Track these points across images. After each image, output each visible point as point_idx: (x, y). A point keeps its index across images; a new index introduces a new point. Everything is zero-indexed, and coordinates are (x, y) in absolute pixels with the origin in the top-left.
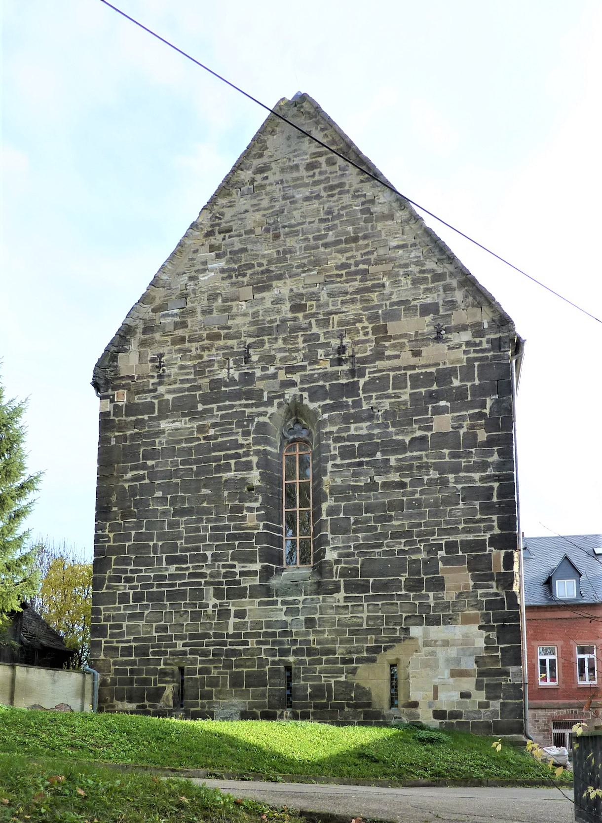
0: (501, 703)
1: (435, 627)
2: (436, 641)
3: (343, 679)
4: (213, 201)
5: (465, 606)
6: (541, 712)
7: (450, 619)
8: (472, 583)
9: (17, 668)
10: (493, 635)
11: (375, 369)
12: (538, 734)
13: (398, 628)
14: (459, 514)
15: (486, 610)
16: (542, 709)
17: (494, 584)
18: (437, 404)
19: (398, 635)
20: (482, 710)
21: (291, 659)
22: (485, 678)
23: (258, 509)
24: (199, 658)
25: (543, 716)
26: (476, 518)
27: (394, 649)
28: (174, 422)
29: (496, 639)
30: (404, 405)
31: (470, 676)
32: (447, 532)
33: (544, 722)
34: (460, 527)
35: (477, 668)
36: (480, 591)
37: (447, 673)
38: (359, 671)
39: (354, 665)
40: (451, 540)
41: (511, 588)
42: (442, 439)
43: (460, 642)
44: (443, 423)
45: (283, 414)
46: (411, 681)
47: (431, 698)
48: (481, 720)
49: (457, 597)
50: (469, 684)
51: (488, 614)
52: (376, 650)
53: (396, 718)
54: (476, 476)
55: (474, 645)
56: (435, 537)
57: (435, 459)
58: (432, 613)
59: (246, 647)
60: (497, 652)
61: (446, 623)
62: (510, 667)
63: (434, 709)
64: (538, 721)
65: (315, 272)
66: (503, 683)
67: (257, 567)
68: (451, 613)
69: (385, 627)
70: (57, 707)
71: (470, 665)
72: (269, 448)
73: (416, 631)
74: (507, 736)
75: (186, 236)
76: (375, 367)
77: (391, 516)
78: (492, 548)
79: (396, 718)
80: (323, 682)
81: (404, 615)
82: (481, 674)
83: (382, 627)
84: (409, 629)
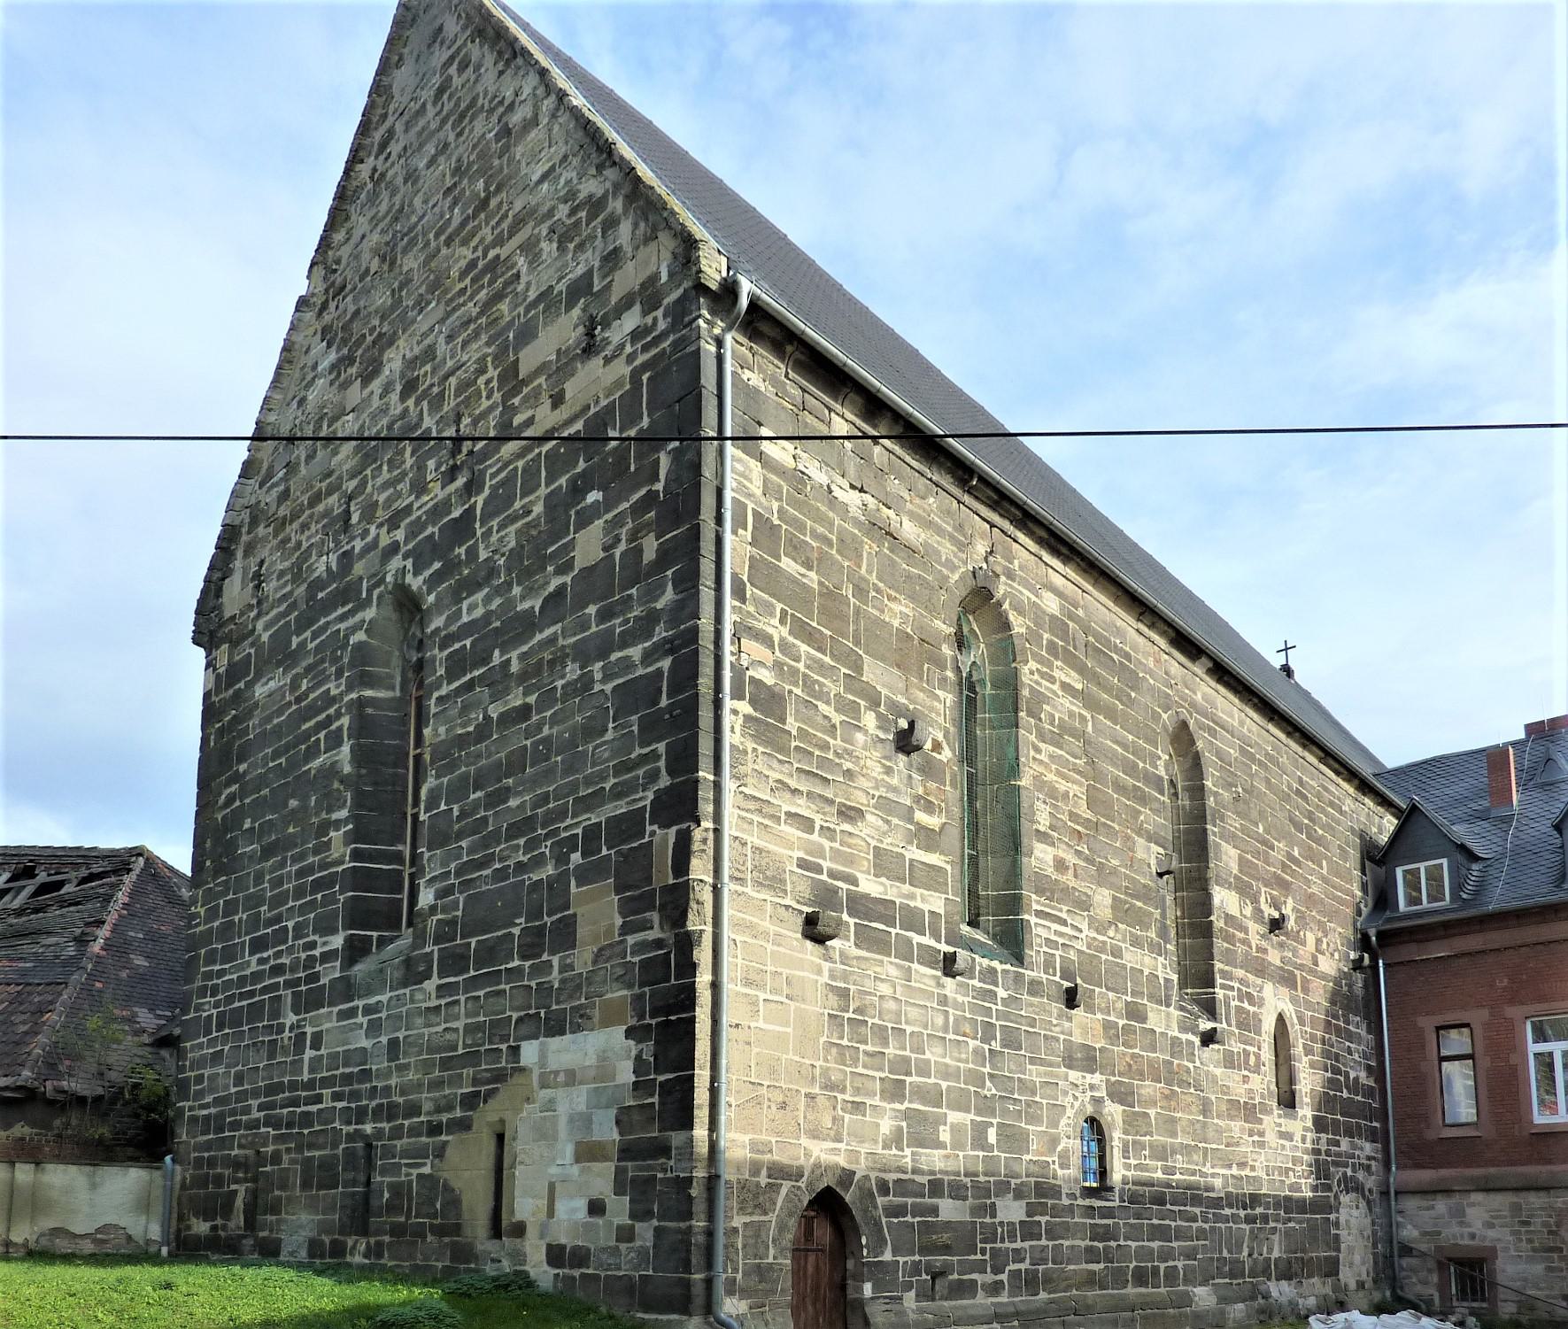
0: (657, 1229)
1: (557, 1039)
2: (556, 1073)
3: (427, 1170)
4: (325, 244)
5: (605, 981)
6: (1536, 1200)
7: (582, 1016)
8: (619, 921)
9: (17, 1165)
10: (648, 1049)
11: (500, 464)
12: (1530, 1260)
13: (504, 1047)
14: (606, 755)
15: (640, 987)
16: (1538, 1189)
17: (655, 917)
18: (582, 505)
19: (504, 1064)
20: (623, 1246)
21: (368, 1128)
22: (630, 1164)
23: (346, 821)
24: (272, 1132)
25: (1542, 1209)
26: (632, 756)
27: (501, 1096)
28: (266, 683)
29: (652, 1059)
30: (534, 527)
31: (606, 1158)
32: (586, 804)
33: (1545, 1224)
34: (608, 786)
35: (616, 1137)
36: (631, 940)
37: (569, 1150)
38: (449, 1152)
39: (443, 1138)
40: (593, 821)
41: (684, 925)
42: (596, 581)
43: (592, 1073)
44: (588, 546)
45: (394, 616)
46: (517, 1173)
47: (543, 1216)
48: (622, 1273)
49: (595, 962)
50: (600, 1181)
51: (642, 995)
52: (471, 1101)
53: (493, 1260)
54: (635, 652)
55: (614, 1080)
56: (569, 822)
57: (575, 634)
58: (554, 1007)
59: (320, 1106)
60: (652, 1095)
61: (577, 1029)
62: (673, 1134)
63: (548, 1240)
64: (1527, 1223)
65: (433, 304)
66: (660, 1175)
67: (337, 941)
68: (583, 1001)
69: (487, 1047)
70: (98, 1231)
71: (607, 1132)
72: (369, 693)
73: (530, 1052)
74: (660, 1317)
75: (293, 328)
76: (498, 460)
77: (508, 789)
78: (655, 827)
79: (493, 1260)
80: (403, 1178)
81: (515, 1016)
82: (627, 1152)
83: (482, 1049)
84: (519, 1047)
